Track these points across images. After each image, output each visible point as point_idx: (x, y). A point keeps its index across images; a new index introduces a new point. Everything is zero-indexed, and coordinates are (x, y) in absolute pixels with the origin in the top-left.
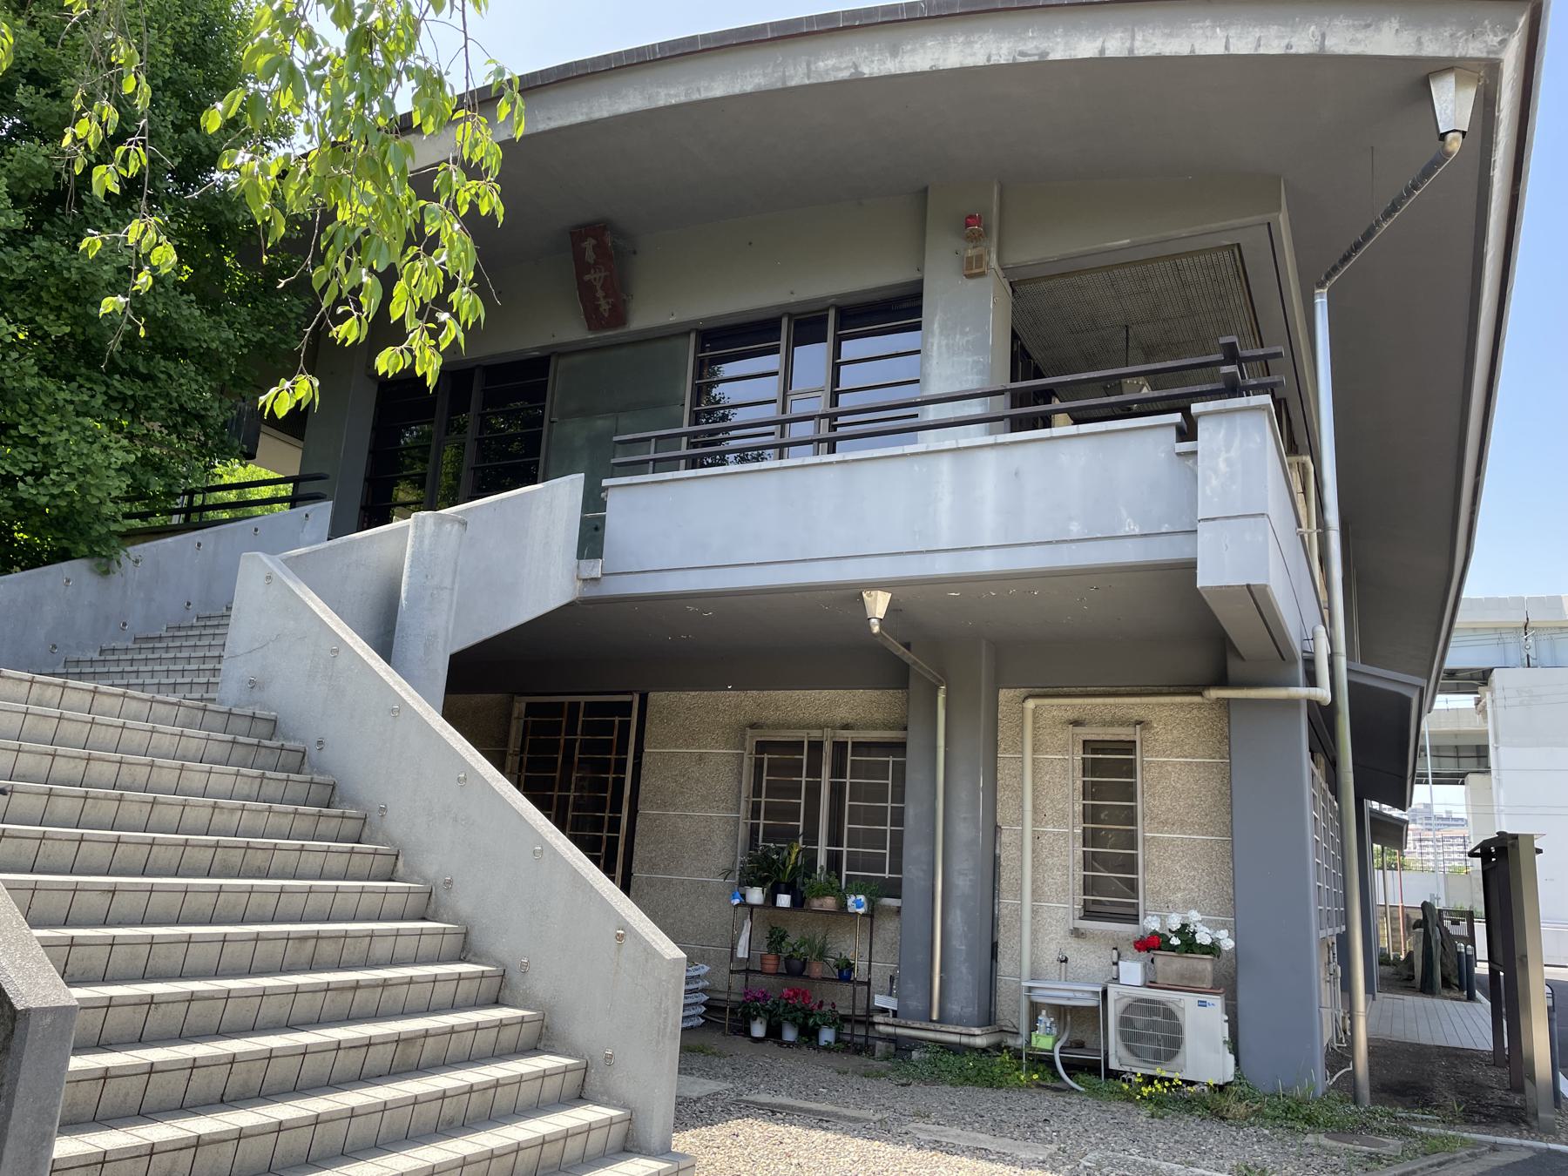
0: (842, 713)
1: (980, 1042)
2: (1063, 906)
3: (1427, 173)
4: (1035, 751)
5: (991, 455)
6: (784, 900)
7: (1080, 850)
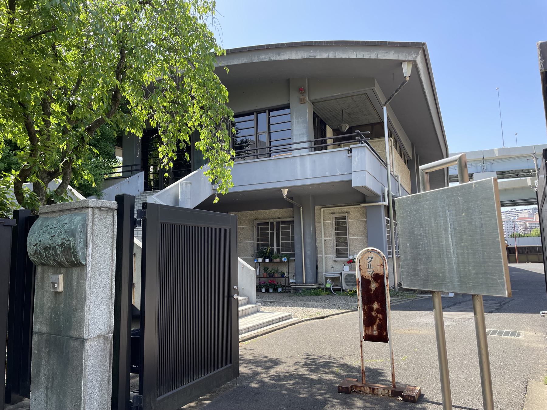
0: (278, 215)
1: (314, 287)
2: (332, 255)
3: (402, 85)
4: (324, 220)
5: (308, 157)
6: (267, 260)
7: (335, 243)
